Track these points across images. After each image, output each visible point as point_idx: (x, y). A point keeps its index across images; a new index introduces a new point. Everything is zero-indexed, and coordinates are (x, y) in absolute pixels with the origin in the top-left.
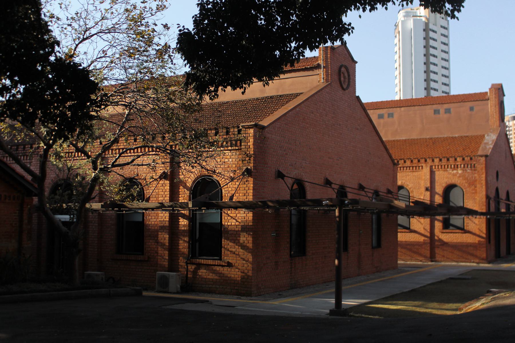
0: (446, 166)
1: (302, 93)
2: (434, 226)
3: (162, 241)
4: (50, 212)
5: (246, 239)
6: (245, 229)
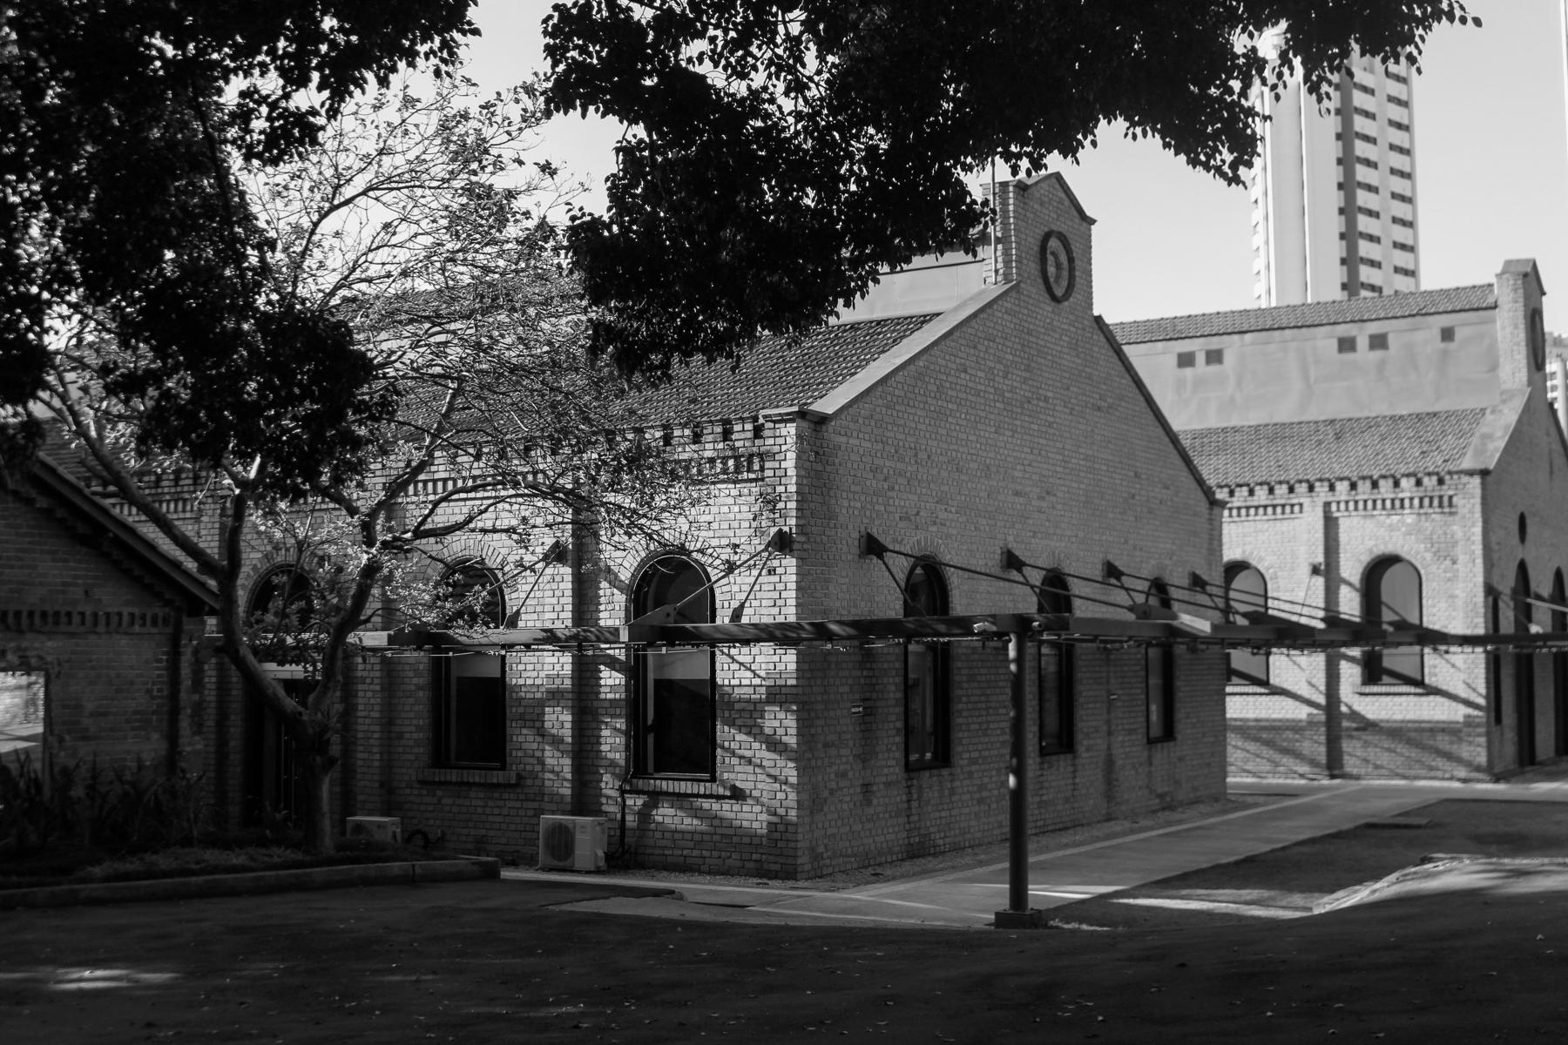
0: (1370, 504)
1: (938, 314)
2: (1338, 676)
3: (554, 731)
4: (251, 658)
5: (783, 723)
6: (777, 695)
